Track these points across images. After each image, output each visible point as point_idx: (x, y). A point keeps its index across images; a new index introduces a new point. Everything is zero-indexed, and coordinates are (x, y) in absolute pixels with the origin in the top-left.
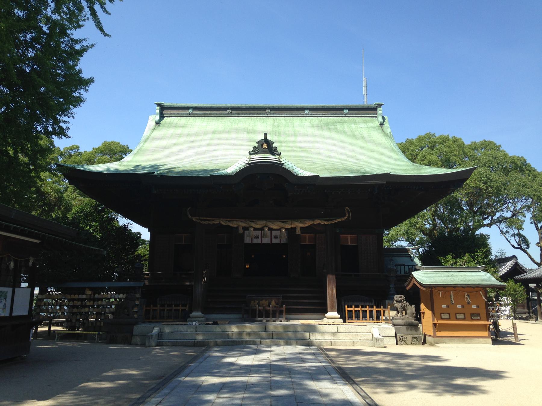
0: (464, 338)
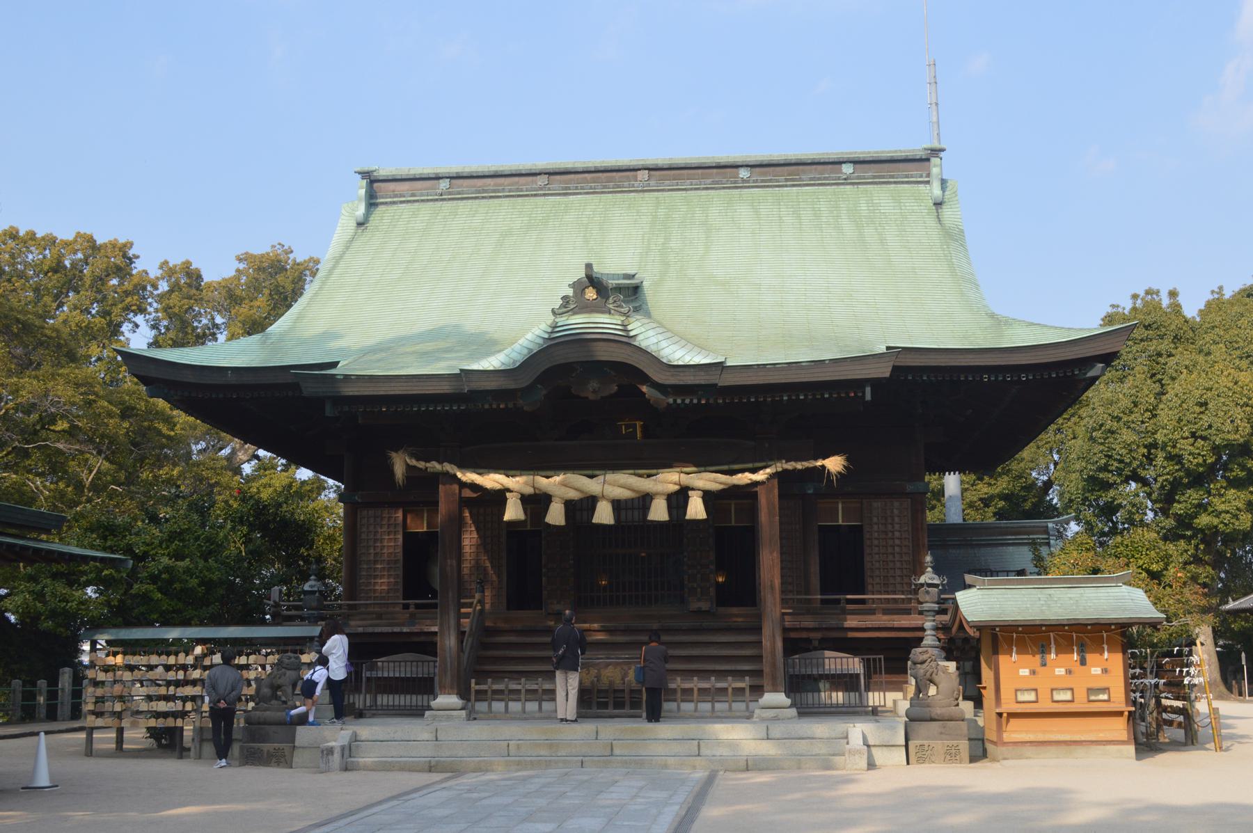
0: (1068, 745)
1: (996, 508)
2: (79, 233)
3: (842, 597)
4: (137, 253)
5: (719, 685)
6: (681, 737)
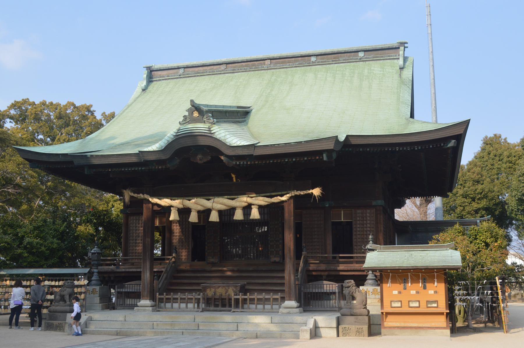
1: (481, 214)
2: (68, 102)
3: (337, 255)
4: (94, 110)
5: (267, 297)
6: (232, 322)
